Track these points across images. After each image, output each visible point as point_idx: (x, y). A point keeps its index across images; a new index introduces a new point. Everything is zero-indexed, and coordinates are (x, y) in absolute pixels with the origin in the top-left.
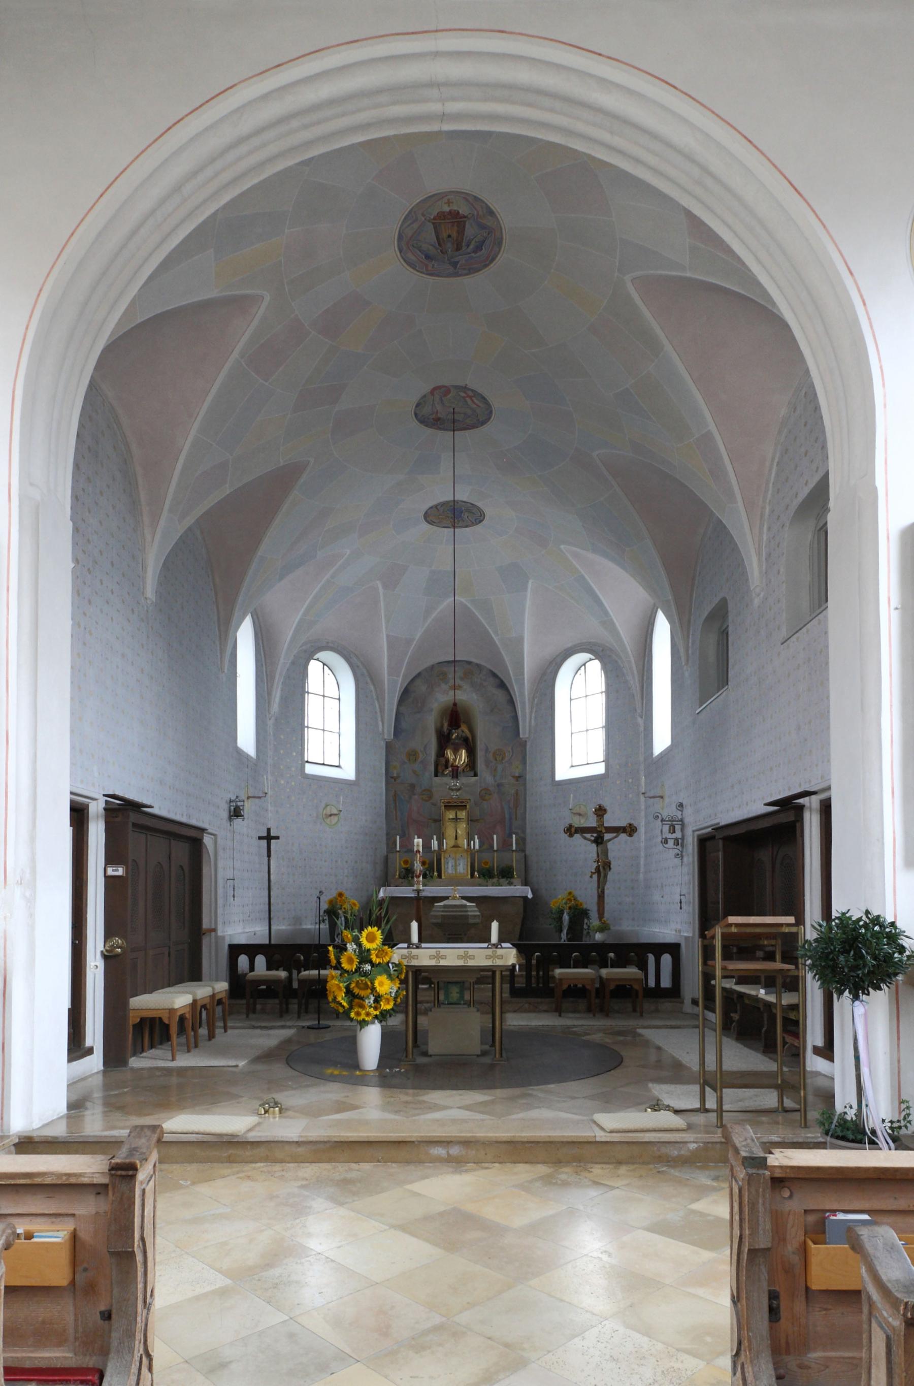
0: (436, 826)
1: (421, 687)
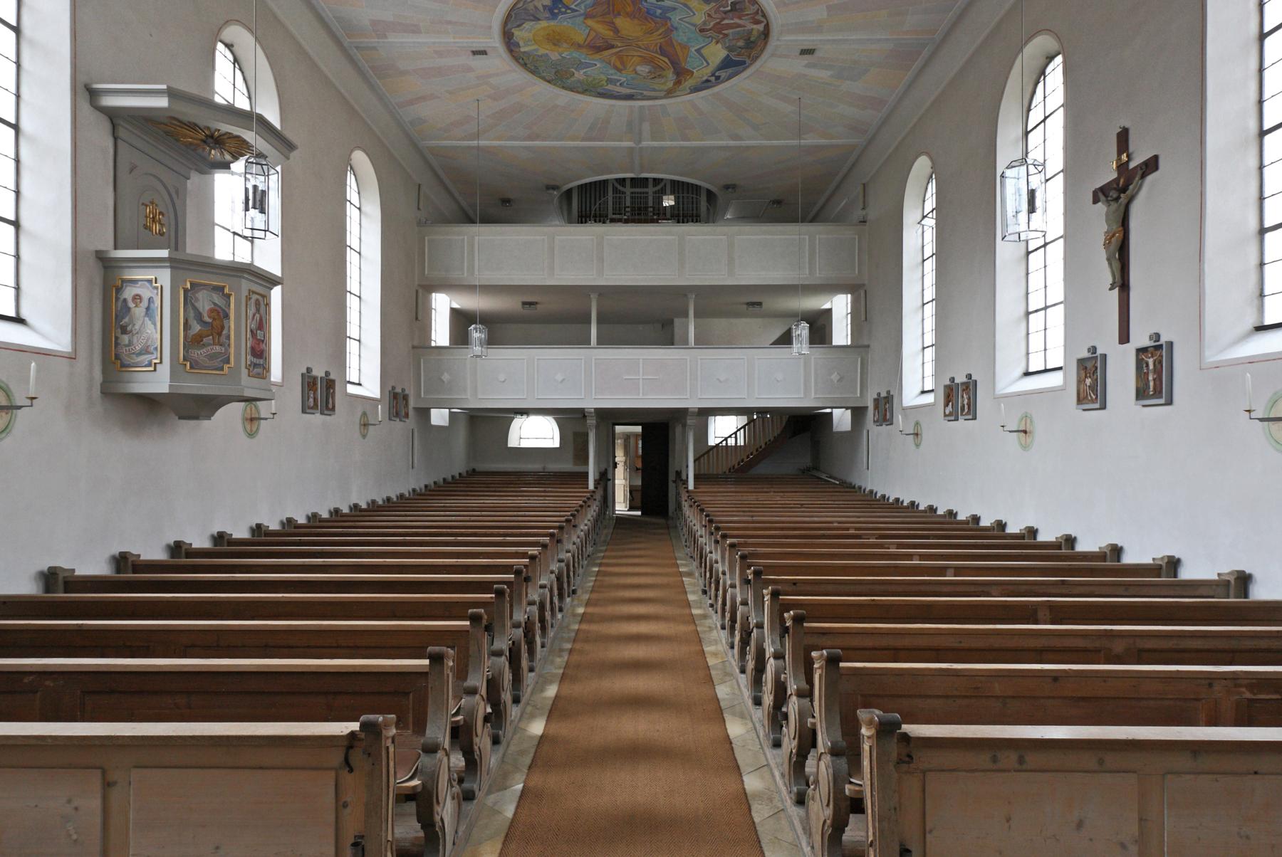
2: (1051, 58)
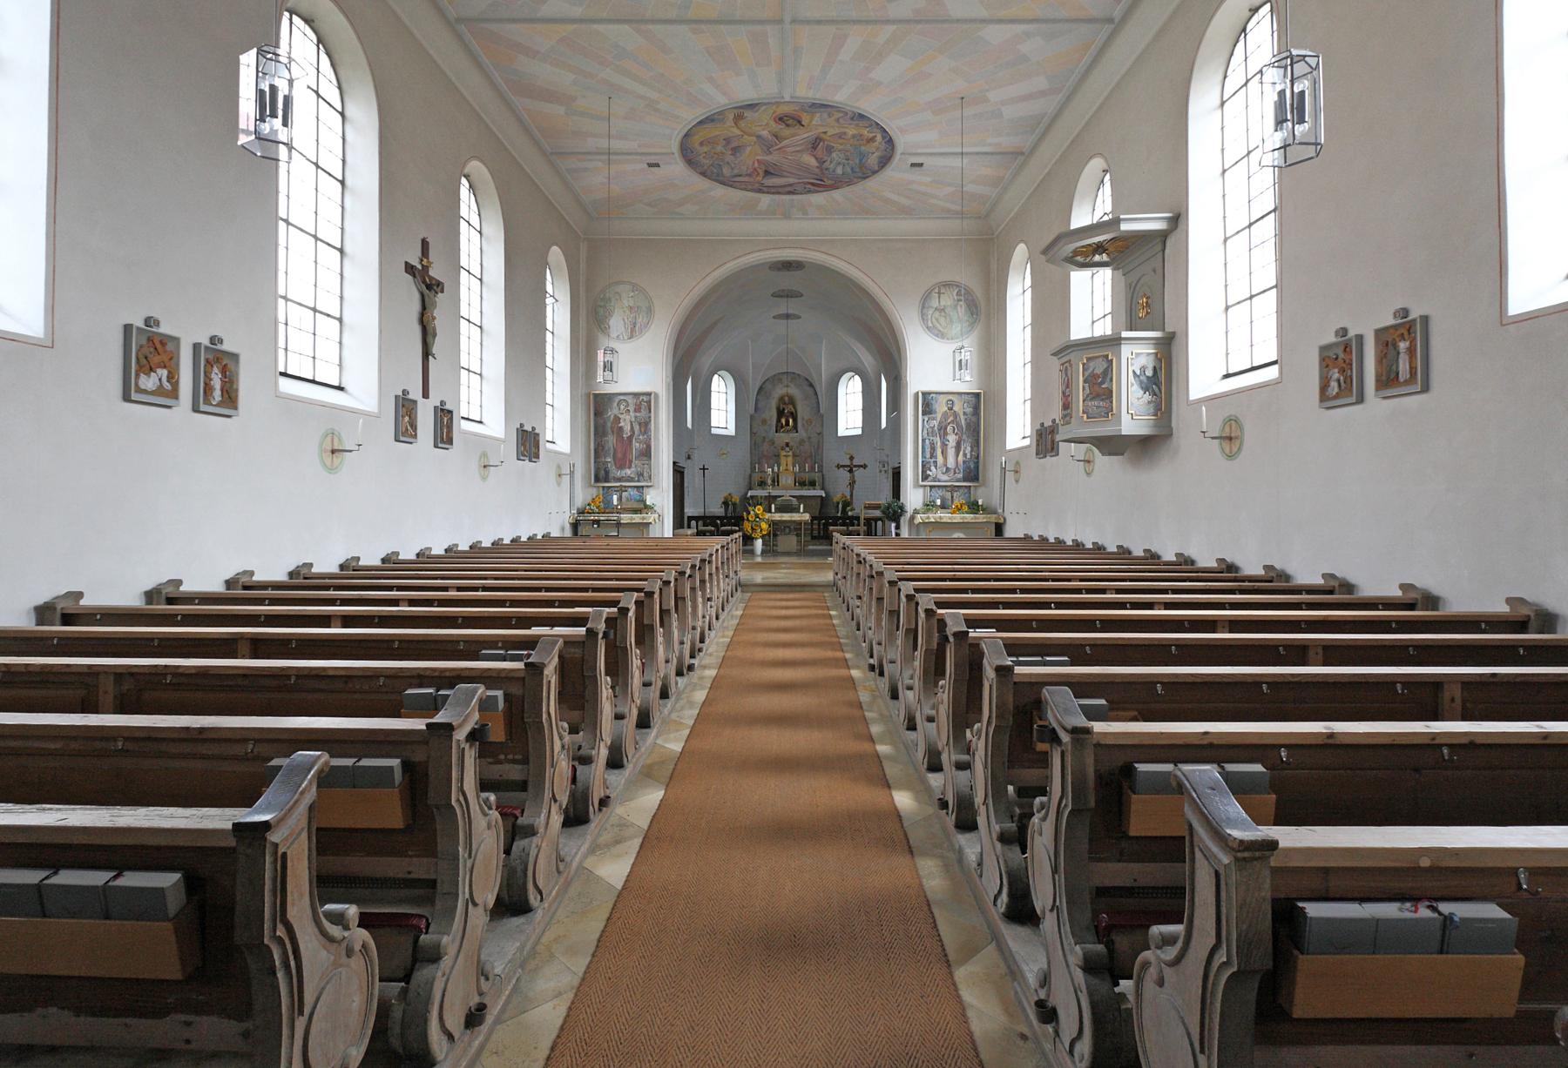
1: (768, 386)
2: (1255, 10)
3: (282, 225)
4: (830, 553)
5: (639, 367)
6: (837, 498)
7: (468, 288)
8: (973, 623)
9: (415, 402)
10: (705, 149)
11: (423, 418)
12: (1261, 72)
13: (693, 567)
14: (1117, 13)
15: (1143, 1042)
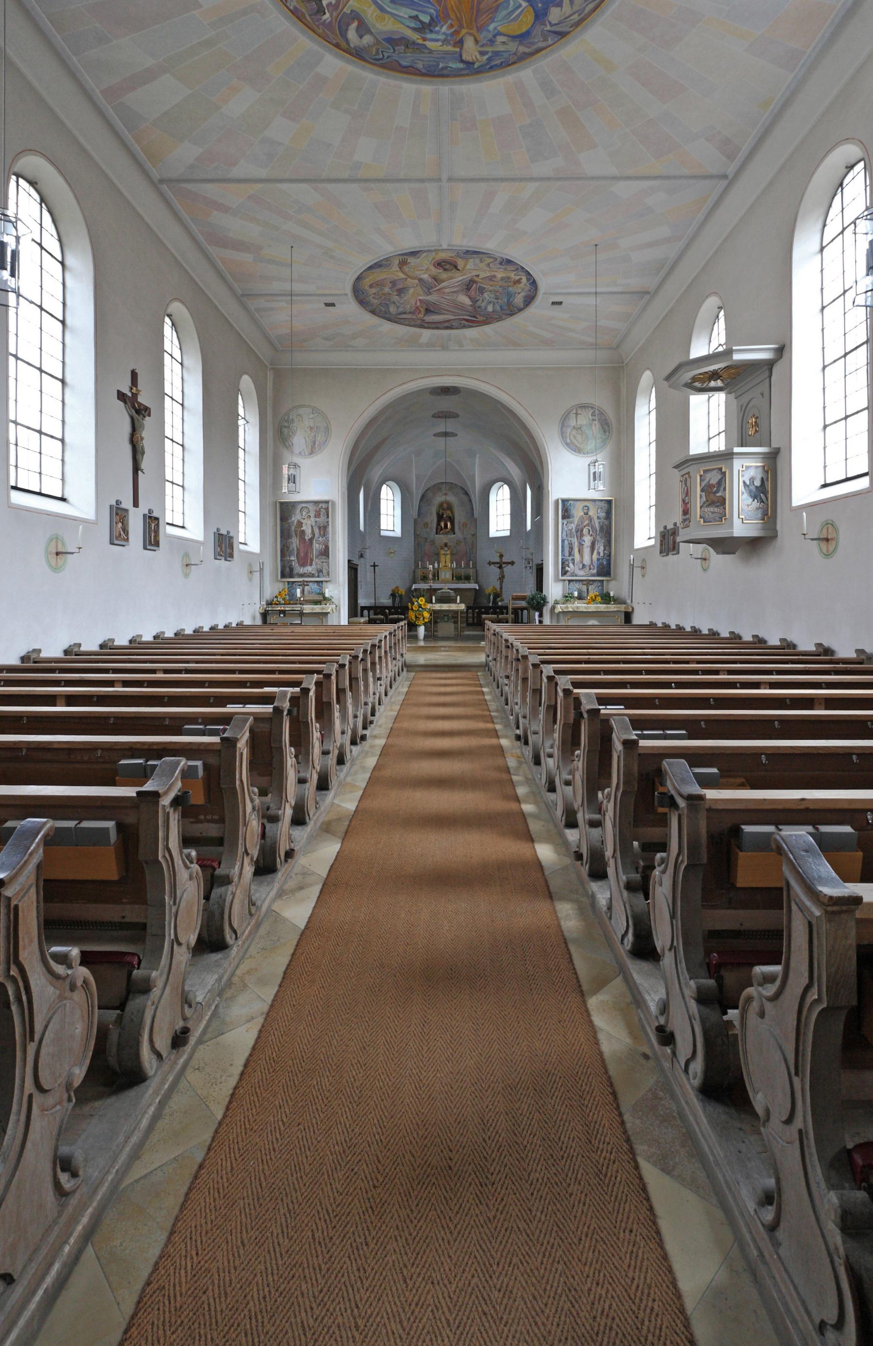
0: (436, 557)
2: (851, 167)
3: (12, 360)
4: (482, 638)
5: (319, 481)
6: (489, 590)
7: (171, 412)
8: (604, 700)
9: (126, 511)
10: (374, 290)
11: (132, 522)
12: (854, 223)
13: (365, 651)
14: (731, 171)
15: (747, 1064)
